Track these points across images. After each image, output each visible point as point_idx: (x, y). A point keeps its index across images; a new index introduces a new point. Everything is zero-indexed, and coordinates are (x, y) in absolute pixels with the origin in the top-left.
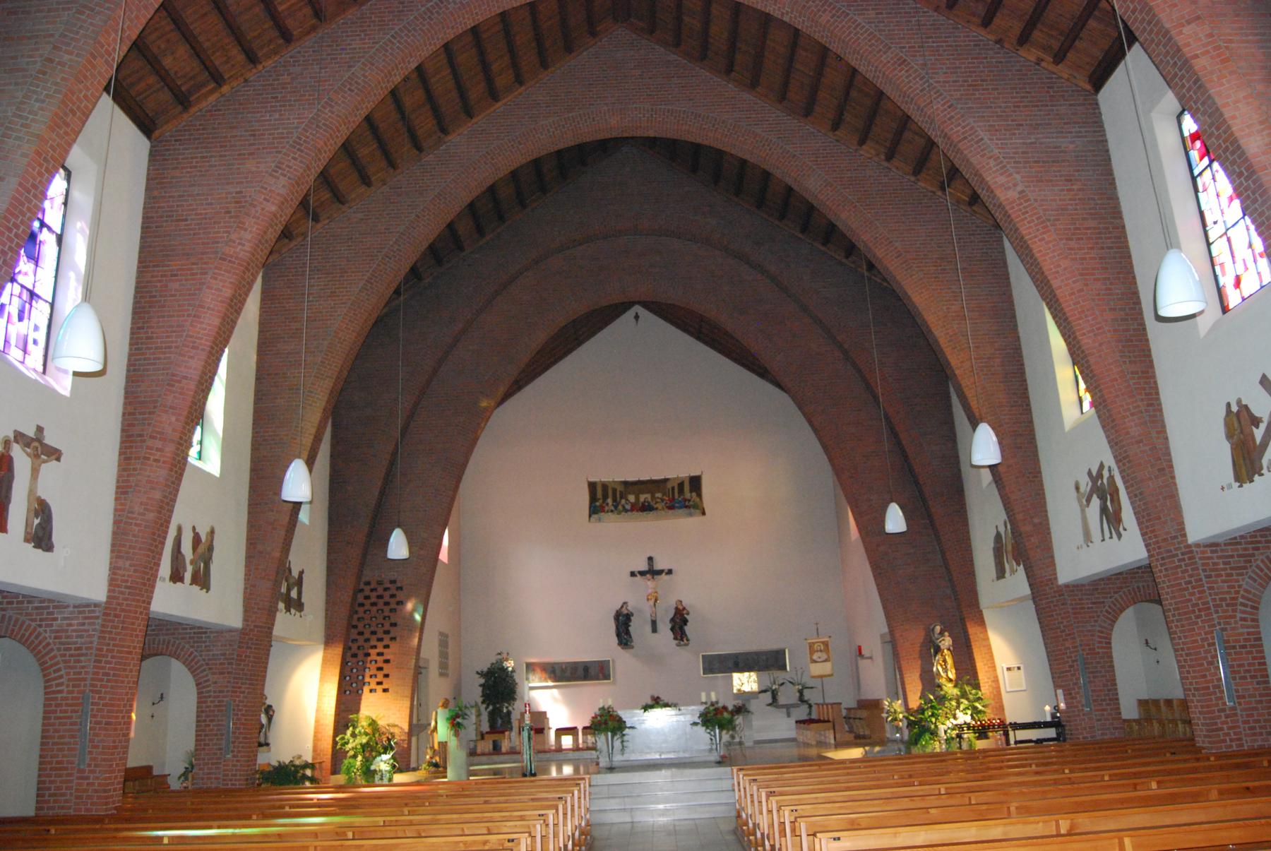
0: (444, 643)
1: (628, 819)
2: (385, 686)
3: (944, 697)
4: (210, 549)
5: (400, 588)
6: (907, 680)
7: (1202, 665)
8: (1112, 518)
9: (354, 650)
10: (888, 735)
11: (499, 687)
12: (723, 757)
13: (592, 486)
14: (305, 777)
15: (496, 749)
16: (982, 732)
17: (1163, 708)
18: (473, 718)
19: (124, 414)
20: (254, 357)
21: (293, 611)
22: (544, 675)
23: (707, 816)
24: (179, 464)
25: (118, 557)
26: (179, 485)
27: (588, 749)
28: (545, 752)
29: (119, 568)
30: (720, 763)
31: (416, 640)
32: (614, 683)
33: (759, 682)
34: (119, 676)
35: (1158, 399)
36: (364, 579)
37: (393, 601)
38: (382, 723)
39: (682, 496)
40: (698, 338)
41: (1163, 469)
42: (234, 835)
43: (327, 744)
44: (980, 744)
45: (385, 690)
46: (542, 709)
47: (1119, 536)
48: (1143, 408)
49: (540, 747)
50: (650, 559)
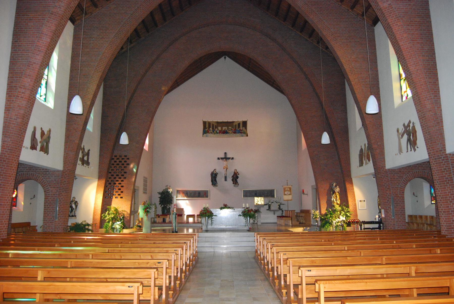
0: (145, 180)
1: (213, 251)
2: (121, 196)
3: (335, 210)
4: (49, 137)
5: (128, 159)
6: (321, 203)
7: (448, 202)
8: (412, 143)
9: (110, 181)
10: (312, 223)
11: (166, 199)
12: (250, 228)
13: (204, 123)
14: (89, 230)
15: (164, 221)
16: (349, 224)
17: (414, 219)
18: (154, 209)
19: (9, 77)
20: (70, 62)
21: (85, 165)
22: (184, 195)
23: (243, 250)
24: (32, 100)
25: (5, 137)
26: (32, 108)
27: (198, 223)
28: (182, 223)
29: (6, 141)
30: (249, 231)
31: (134, 179)
32: (210, 199)
33: (264, 201)
34: (5, 185)
35: (439, 94)
36: (114, 154)
37: (125, 163)
38: (120, 210)
39: (239, 128)
40: (248, 70)
41: (439, 123)
42: (40, 254)
43: (98, 217)
44: (348, 229)
45: (121, 198)
46: (182, 207)
47: (415, 150)
48: (432, 97)
49: (180, 221)
50: (225, 153)
